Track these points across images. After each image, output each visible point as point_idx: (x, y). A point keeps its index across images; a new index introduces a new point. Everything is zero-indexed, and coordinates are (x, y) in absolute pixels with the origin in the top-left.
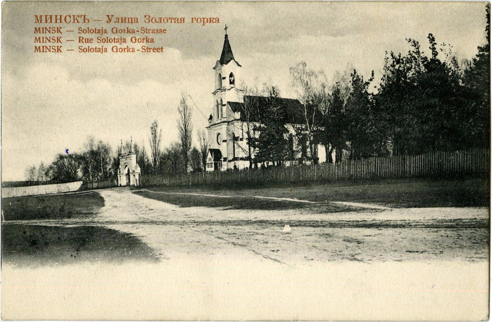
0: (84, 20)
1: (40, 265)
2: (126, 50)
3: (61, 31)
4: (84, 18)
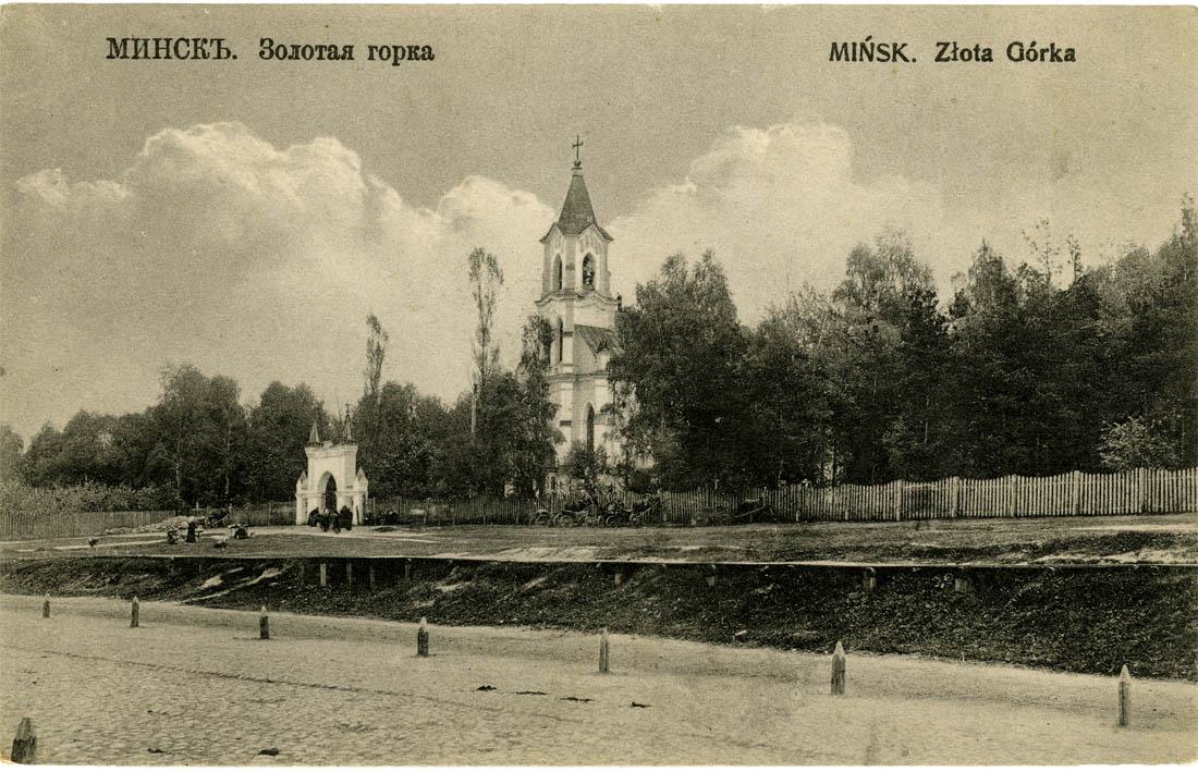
0: (219, 52)
2: (1048, 56)
3: (905, 54)
4: (219, 44)
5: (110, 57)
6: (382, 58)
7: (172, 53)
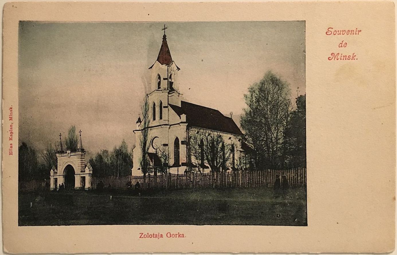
2: (177, 236)
5: (12, 120)
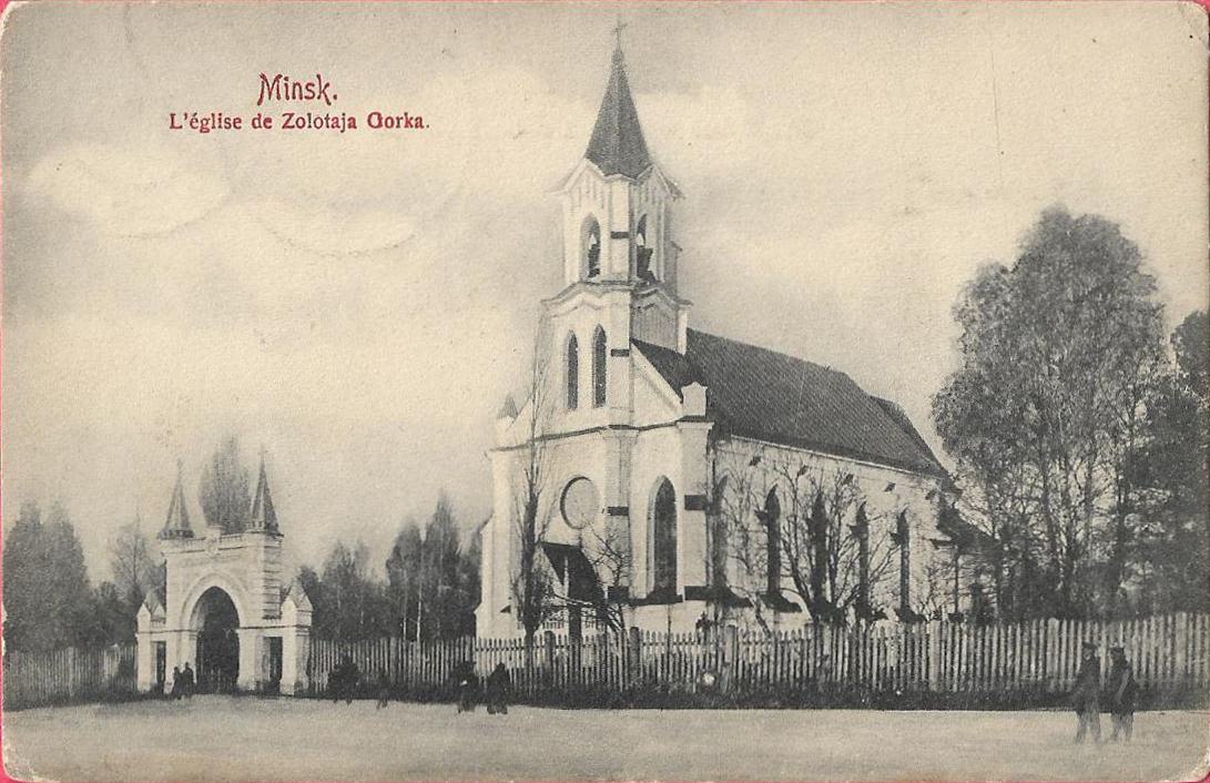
1: (1021, 252)
2: (403, 122)
6: (370, 124)
7: (312, 124)
